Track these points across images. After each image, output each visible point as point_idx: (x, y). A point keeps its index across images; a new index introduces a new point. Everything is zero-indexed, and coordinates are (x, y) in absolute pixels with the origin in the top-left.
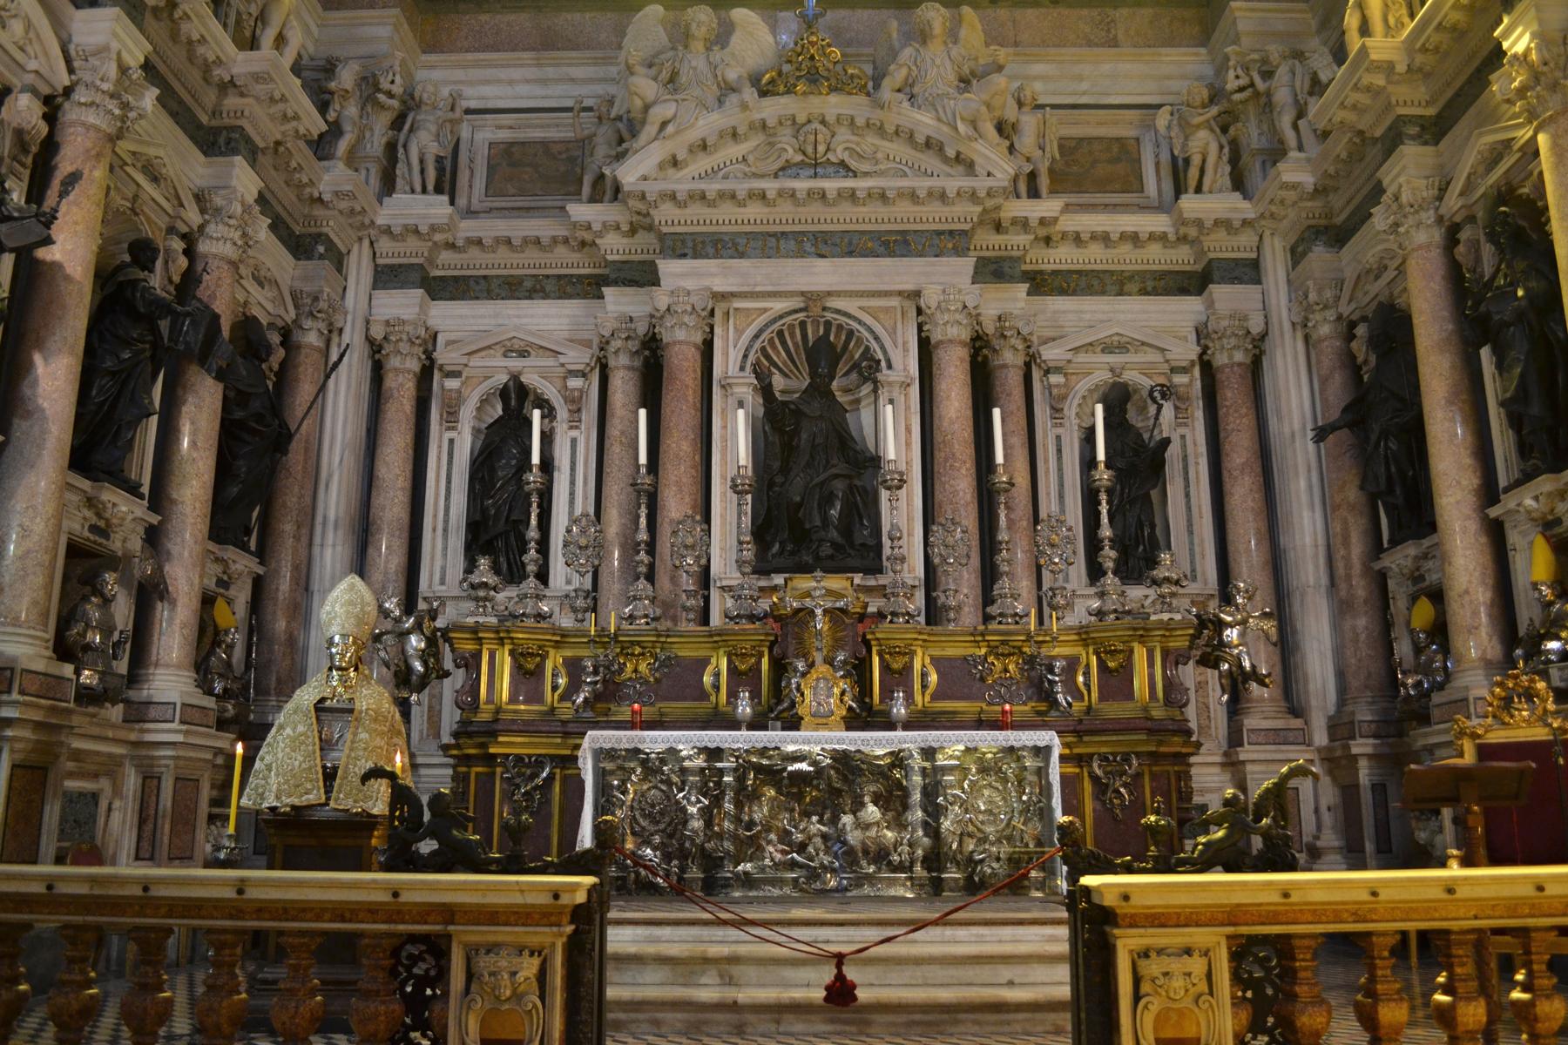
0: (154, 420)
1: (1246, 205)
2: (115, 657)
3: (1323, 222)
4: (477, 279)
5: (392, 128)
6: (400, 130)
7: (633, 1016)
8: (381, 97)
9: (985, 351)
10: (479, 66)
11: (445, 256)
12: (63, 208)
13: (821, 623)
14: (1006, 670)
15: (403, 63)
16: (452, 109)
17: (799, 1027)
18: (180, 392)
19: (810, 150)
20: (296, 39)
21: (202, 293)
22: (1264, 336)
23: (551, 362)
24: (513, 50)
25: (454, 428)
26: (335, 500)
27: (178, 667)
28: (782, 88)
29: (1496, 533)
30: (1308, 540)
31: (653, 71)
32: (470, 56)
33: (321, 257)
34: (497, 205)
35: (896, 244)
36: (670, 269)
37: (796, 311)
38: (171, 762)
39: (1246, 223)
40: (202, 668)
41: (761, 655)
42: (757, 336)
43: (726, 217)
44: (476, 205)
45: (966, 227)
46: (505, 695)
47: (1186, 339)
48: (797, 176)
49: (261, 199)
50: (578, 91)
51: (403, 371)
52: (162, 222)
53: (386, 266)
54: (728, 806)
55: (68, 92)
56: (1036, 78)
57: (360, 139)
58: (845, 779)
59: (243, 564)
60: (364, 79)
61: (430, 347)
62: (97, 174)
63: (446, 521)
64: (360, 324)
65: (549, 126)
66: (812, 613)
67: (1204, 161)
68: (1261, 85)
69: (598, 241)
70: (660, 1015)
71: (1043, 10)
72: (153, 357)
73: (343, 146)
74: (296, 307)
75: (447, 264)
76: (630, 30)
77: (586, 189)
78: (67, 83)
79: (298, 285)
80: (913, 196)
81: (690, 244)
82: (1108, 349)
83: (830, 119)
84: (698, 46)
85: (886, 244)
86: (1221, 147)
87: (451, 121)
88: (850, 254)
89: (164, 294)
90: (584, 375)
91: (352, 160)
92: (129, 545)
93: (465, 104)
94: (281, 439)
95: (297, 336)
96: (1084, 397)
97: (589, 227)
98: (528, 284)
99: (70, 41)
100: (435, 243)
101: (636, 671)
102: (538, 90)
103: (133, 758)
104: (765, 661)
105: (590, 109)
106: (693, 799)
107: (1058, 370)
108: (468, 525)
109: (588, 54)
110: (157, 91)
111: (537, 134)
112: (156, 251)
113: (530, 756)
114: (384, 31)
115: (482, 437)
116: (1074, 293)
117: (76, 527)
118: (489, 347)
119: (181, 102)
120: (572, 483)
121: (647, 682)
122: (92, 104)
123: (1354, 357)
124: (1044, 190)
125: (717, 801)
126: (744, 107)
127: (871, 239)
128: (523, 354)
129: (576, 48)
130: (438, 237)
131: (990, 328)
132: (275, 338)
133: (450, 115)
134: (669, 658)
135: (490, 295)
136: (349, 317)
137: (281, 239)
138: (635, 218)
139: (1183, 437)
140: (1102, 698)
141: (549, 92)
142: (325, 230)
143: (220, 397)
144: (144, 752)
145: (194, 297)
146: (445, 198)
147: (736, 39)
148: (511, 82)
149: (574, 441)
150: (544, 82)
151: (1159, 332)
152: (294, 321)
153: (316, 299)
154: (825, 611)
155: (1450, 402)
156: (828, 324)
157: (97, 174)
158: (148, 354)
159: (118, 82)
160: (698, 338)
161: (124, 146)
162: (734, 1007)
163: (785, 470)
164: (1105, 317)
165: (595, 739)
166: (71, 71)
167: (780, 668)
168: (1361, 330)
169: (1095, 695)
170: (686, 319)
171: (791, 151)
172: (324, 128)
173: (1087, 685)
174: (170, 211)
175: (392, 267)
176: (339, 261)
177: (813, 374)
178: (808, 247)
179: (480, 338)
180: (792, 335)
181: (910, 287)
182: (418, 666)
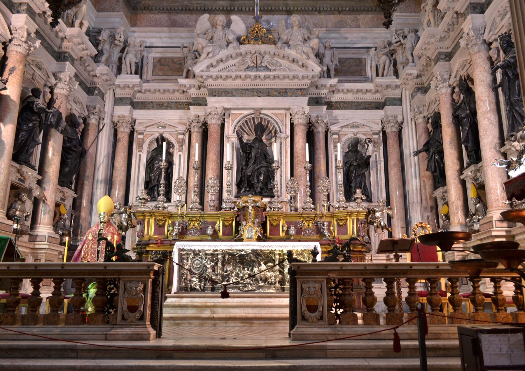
0: (40, 146)
1: (397, 80)
2: (25, 220)
3: (421, 86)
4: (149, 103)
5: (120, 52)
6: (123, 53)
7: (183, 321)
8: (116, 42)
9: (312, 127)
10: (149, 32)
11: (138, 95)
12: (10, 78)
13: (251, 210)
14: (309, 226)
15: (124, 31)
16: (141, 46)
17: (233, 324)
18: (49, 137)
19: (255, 62)
20: (86, 24)
21: (56, 105)
22: (402, 123)
23: (173, 130)
24: (162, 27)
26: (101, 174)
27: (47, 224)
28: (247, 42)
29: (463, 183)
30: (414, 188)
31: (206, 36)
32: (147, 29)
33: (97, 95)
34: (156, 78)
35: (283, 93)
36: (212, 101)
37: (251, 114)
38: (44, 255)
39: (397, 86)
40: (56, 226)
41: (233, 221)
42: (238, 122)
43: (230, 84)
44: (149, 79)
45: (306, 87)
46: (152, 233)
47: (378, 124)
48: (252, 71)
49: (76, 76)
50: (182, 41)
51: (124, 132)
52: (42, 83)
53: (118, 98)
54: (220, 265)
55: (10, 41)
56: (332, 38)
57: (110, 56)
58: (256, 257)
59: (70, 194)
60: (111, 36)
61: (133, 125)
62: (20, 67)
63: (138, 181)
64: (109, 116)
65: (173, 52)
66: (248, 207)
67: (385, 66)
68: (402, 41)
69: (188, 91)
70: (191, 321)
71: (336, 16)
72: (39, 126)
73: (104, 58)
74: (88, 111)
75: (139, 97)
76: (199, 22)
77: (185, 74)
78: (10, 38)
79: (89, 104)
80: (288, 77)
81: (217, 92)
82: (353, 127)
83: (262, 52)
84: (219, 28)
85: (280, 93)
86: (390, 61)
87: (140, 51)
88: (268, 96)
89: (43, 106)
90: (184, 134)
91: (107, 63)
92: (31, 185)
93: (145, 45)
94: (83, 154)
95: (88, 120)
96: (344, 142)
97: (185, 87)
98: (166, 105)
99: (11, 24)
100: (135, 91)
101: (194, 225)
102: (170, 41)
103: (31, 253)
104: (234, 223)
105: (186, 47)
106: (209, 263)
107: (336, 134)
108: (145, 182)
109: (187, 29)
110: (40, 41)
111: (169, 55)
112: (40, 92)
113: (159, 251)
114: (117, 20)
116: (342, 109)
117: (14, 179)
118: (153, 125)
119: (48, 44)
120: (179, 169)
121: (197, 229)
122: (19, 45)
123: (429, 129)
124: (332, 76)
125: (216, 264)
126: (234, 48)
127: (275, 91)
128: (164, 127)
129: (182, 27)
130: (136, 89)
131: (314, 120)
132: (81, 121)
133: (140, 49)
134: (204, 221)
135: (153, 108)
136: (106, 115)
137: (83, 89)
138: (200, 84)
139: (376, 155)
140: (338, 234)
141: (174, 41)
142: (98, 86)
143: (62, 139)
144: (35, 251)
145: (53, 107)
146: (138, 76)
147: (232, 26)
149: (180, 156)
150: (171, 38)
151: (369, 122)
152: (88, 115)
153: (95, 108)
154: (252, 207)
155: (450, 143)
156: (261, 118)
157: (21, 67)
158: (38, 125)
159: (27, 38)
160: (219, 122)
161: (29, 58)
162: (213, 319)
163: (247, 165)
164: (352, 117)
165: (179, 245)
166: (11, 34)
167: (238, 224)
168: (430, 121)
169: (336, 233)
170: (215, 116)
171: (250, 63)
172: (97, 53)
173: (333, 230)
174: (45, 79)
175: (120, 98)
176: (103, 96)
177: (256, 134)
178: (255, 93)
179: (152, 123)
180: (250, 122)
181: (287, 106)
182: (125, 224)
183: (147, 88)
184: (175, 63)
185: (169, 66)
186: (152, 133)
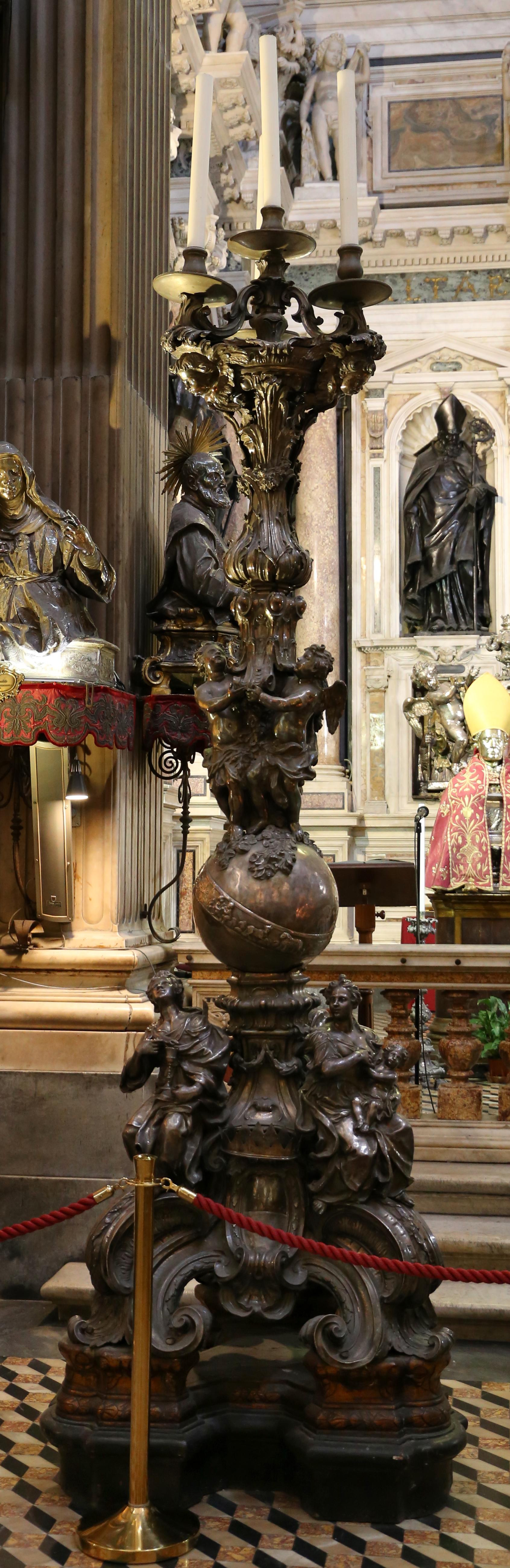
25: (379, 456)
65: (459, 77)
98: (453, 282)
102: (444, 31)
111: (445, 89)
115: (412, 464)
148: (411, 22)
183: (394, 227)
184: (467, 118)
185: (445, 130)
186: (413, 389)
